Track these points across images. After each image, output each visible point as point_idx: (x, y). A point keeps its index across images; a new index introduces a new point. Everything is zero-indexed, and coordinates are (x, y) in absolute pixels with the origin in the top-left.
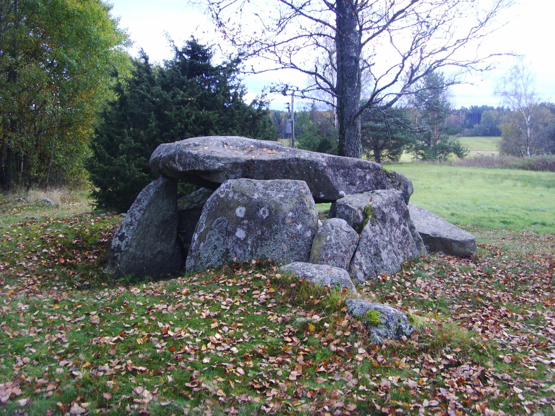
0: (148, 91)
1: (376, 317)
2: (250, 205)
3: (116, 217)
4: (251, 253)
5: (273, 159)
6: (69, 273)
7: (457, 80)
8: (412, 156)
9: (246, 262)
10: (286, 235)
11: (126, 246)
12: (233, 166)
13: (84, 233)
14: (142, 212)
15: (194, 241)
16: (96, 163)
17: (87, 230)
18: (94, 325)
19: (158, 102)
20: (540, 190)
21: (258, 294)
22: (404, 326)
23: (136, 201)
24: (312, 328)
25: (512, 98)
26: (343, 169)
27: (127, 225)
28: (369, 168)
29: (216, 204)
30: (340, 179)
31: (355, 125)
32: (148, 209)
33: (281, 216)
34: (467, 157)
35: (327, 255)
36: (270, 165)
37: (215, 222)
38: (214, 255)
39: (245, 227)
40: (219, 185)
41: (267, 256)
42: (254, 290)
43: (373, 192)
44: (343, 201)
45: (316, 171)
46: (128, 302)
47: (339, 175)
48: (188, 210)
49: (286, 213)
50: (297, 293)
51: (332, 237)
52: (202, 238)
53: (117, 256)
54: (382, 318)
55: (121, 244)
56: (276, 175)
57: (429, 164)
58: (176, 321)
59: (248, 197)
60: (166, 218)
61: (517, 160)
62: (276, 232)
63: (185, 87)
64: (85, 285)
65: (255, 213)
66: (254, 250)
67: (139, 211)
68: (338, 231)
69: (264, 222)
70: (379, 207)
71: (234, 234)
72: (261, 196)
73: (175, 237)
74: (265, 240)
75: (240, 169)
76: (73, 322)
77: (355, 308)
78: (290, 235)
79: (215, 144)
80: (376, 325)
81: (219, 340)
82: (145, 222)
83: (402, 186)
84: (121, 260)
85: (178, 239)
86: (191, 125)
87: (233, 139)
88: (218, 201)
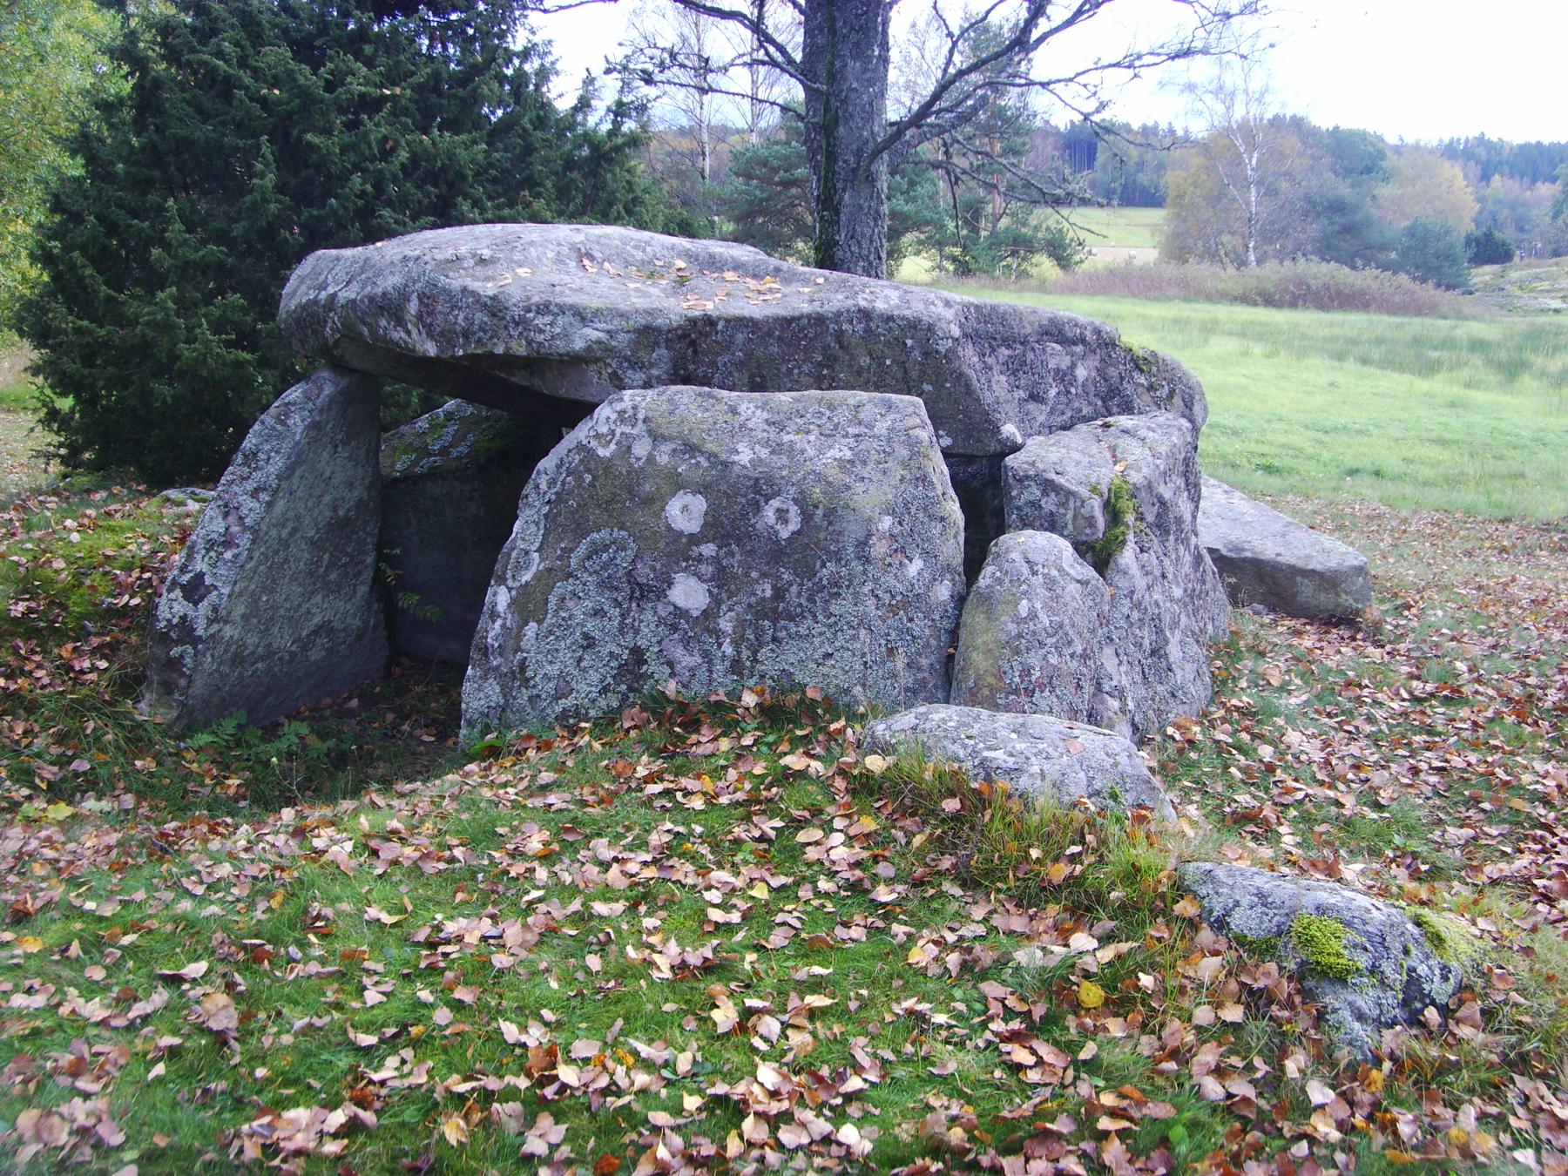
0: (243, 64)
1: (1336, 946)
2: (724, 487)
3: (150, 505)
4: (736, 667)
5: (782, 312)
6: (11, 730)
7: (1198, 44)
8: (929, 264)
9: (718, 704)
10: (871, 602)
11: (211, 622)
12: (637, 342)
13: (49, 572)
14: (264, 497)
15: (494, 615)
16: (63, 318)
17: (59, 564)
18: (221, 1039)
19: (279, 102)
20: (1318, 371)
21: (817, 843)
22: (1422, 970)
23: (239, 459)
24: (1092, 994)
25: (1208, 98)
26: (1009, 347)
27: (211, 545)
28: (1083, 341)
29: (580, 479)
30: (1000, 381)
31: (871, 179)
32: (285, 485)
33: (853, 531)
34: (1084, 266)
35: (1026, 672)
36: (770, 334)
37: (582, 549)
38: (584, 670)
39: (707, 570)
40: (588, 409)
41: (799, 677)
42: (799, 824)
43: (1106, 426)
44: (1033, 464)
45: (926, 354)
46: (328, 912)
47: (997, 368)
48: (408, 479)
49: (870, 519)
50: (961, 834)
51: (1038, 606)
52: (528, 605)
53: (182, 657)
54: (1355, 946)
55: (191, 613)
56: (790, 371)
57: (983, 287)
58: (564, 1006)
59: (711, 456)
60: (341, 513)
61: (1227, 277)
62: (834, 588)
63: (368, 49)
64: (77, 775)
65: (745, 517)
66: (745, 654)
67: (255, 494)
68: (1054, 581)
69: (780, 554)
70: (1150, 482)
71: (661, 594)
72: (764, 453)
73: (368, 575)
74: (792, 619)
75: (663, 351)
76: (120, 1022)
77: (1237, 904)
78: (886, 598)
79: (550, 255)
80: (1340, 978)
81: (774, 1094)
82: (274, 533)
83: (1177, 400)
84: (195, 670)
85: (378, 579)
86: (395, 180)
87: (607, 236)
88: (589, 471)
